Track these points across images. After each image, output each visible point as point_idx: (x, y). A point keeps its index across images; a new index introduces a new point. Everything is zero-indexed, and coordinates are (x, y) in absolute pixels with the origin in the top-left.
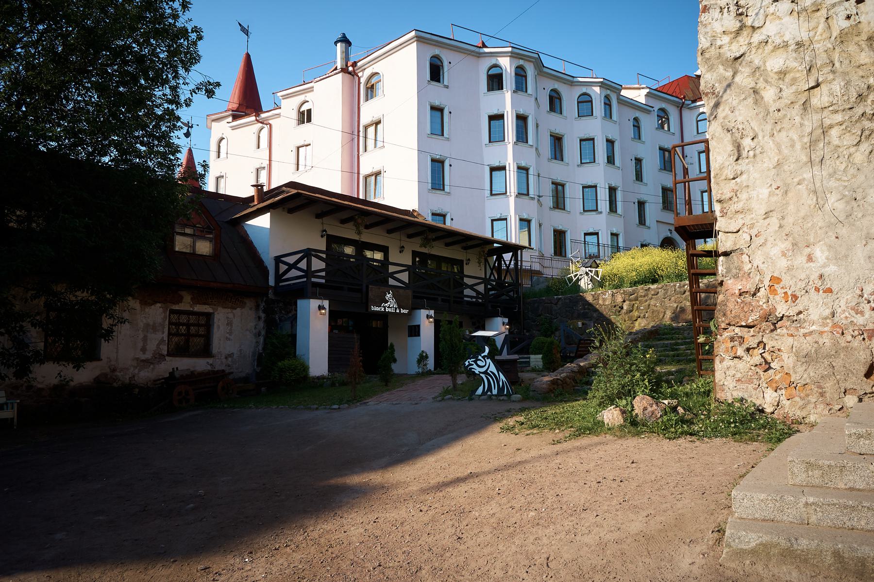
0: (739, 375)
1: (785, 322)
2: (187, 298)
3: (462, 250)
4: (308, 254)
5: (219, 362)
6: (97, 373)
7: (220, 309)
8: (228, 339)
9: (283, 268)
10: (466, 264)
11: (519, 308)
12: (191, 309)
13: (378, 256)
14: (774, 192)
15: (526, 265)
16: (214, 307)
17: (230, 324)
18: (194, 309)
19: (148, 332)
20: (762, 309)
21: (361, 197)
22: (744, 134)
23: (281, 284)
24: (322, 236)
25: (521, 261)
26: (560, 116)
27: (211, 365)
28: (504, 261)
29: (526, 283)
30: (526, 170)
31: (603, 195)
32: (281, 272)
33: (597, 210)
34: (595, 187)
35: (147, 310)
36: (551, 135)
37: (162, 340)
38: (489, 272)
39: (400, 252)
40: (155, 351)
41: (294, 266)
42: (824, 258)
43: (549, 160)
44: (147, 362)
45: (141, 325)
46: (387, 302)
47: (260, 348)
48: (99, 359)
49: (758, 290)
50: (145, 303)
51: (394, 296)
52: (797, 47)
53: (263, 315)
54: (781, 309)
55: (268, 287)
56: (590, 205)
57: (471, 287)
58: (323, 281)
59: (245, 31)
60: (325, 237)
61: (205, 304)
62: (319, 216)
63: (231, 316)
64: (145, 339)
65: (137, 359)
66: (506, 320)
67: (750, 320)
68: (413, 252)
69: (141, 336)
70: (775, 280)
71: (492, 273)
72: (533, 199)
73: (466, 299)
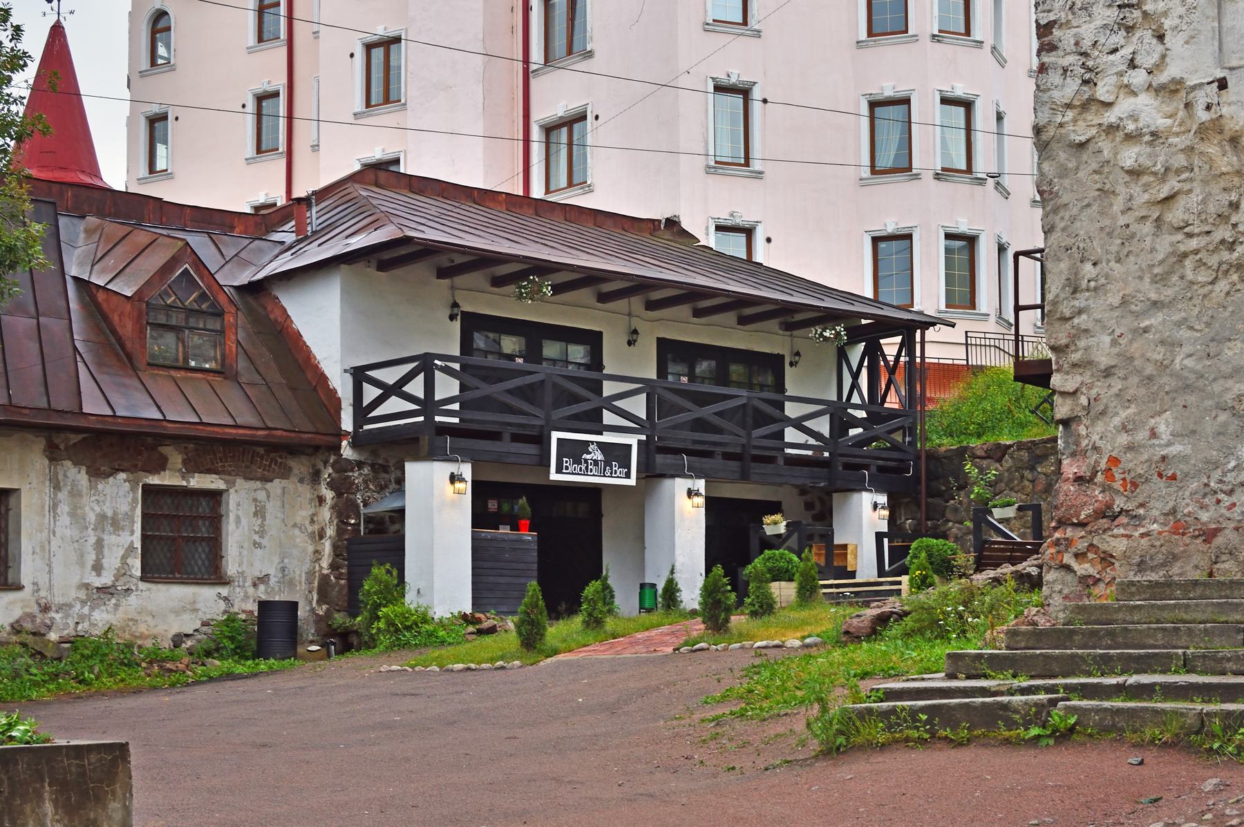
0: (1066, 591)
1: (1123, 519)
2: (176, 458)
3: (781, 332)
4: (425, 365)
5: (242, 594)
7: (240, 482)
8: (257, 545)
9: (371, 393)
10: (791, 364)
12: (184, 483)
13: (578, 353)
14: (1116, 340)
16: (227, 477)
17: (260, 512)
18: (188, 482)
19: (103, 531)
20: (1096, 501)
21: (537, 192)
22: (1085, 255)
23: (366, 427)
24: (452, 318)
25: (923, 342)
27: (226, 599)
28: (884, 356)
30: (967, 105)
35: (100, 487)
37: (131, 548)
38: (847, 381)
39: (630, 343)
40: (118, 570)
41: (395, 390)
42: (1168, 433)
44: (106, 591)
45: (92, 517)
47: (325, 563)
49: (1095, 473)
50: (96, 473)
52: (1151, 139)
53: (329, 495)
54: (1119, 503)
55: (340, 434)
57: (798, 424)
58: (456, 420)
60: (459, 317)
61: (209, 471)
62: (442, 273)
63: (261, 495)
64: (99, 545)
65: (87, 586)
67: (1082, 517)
68: (661, 342)
69: (92, 540)
70: (1114, 461)
72: (981, 182)
73: (788, 451)
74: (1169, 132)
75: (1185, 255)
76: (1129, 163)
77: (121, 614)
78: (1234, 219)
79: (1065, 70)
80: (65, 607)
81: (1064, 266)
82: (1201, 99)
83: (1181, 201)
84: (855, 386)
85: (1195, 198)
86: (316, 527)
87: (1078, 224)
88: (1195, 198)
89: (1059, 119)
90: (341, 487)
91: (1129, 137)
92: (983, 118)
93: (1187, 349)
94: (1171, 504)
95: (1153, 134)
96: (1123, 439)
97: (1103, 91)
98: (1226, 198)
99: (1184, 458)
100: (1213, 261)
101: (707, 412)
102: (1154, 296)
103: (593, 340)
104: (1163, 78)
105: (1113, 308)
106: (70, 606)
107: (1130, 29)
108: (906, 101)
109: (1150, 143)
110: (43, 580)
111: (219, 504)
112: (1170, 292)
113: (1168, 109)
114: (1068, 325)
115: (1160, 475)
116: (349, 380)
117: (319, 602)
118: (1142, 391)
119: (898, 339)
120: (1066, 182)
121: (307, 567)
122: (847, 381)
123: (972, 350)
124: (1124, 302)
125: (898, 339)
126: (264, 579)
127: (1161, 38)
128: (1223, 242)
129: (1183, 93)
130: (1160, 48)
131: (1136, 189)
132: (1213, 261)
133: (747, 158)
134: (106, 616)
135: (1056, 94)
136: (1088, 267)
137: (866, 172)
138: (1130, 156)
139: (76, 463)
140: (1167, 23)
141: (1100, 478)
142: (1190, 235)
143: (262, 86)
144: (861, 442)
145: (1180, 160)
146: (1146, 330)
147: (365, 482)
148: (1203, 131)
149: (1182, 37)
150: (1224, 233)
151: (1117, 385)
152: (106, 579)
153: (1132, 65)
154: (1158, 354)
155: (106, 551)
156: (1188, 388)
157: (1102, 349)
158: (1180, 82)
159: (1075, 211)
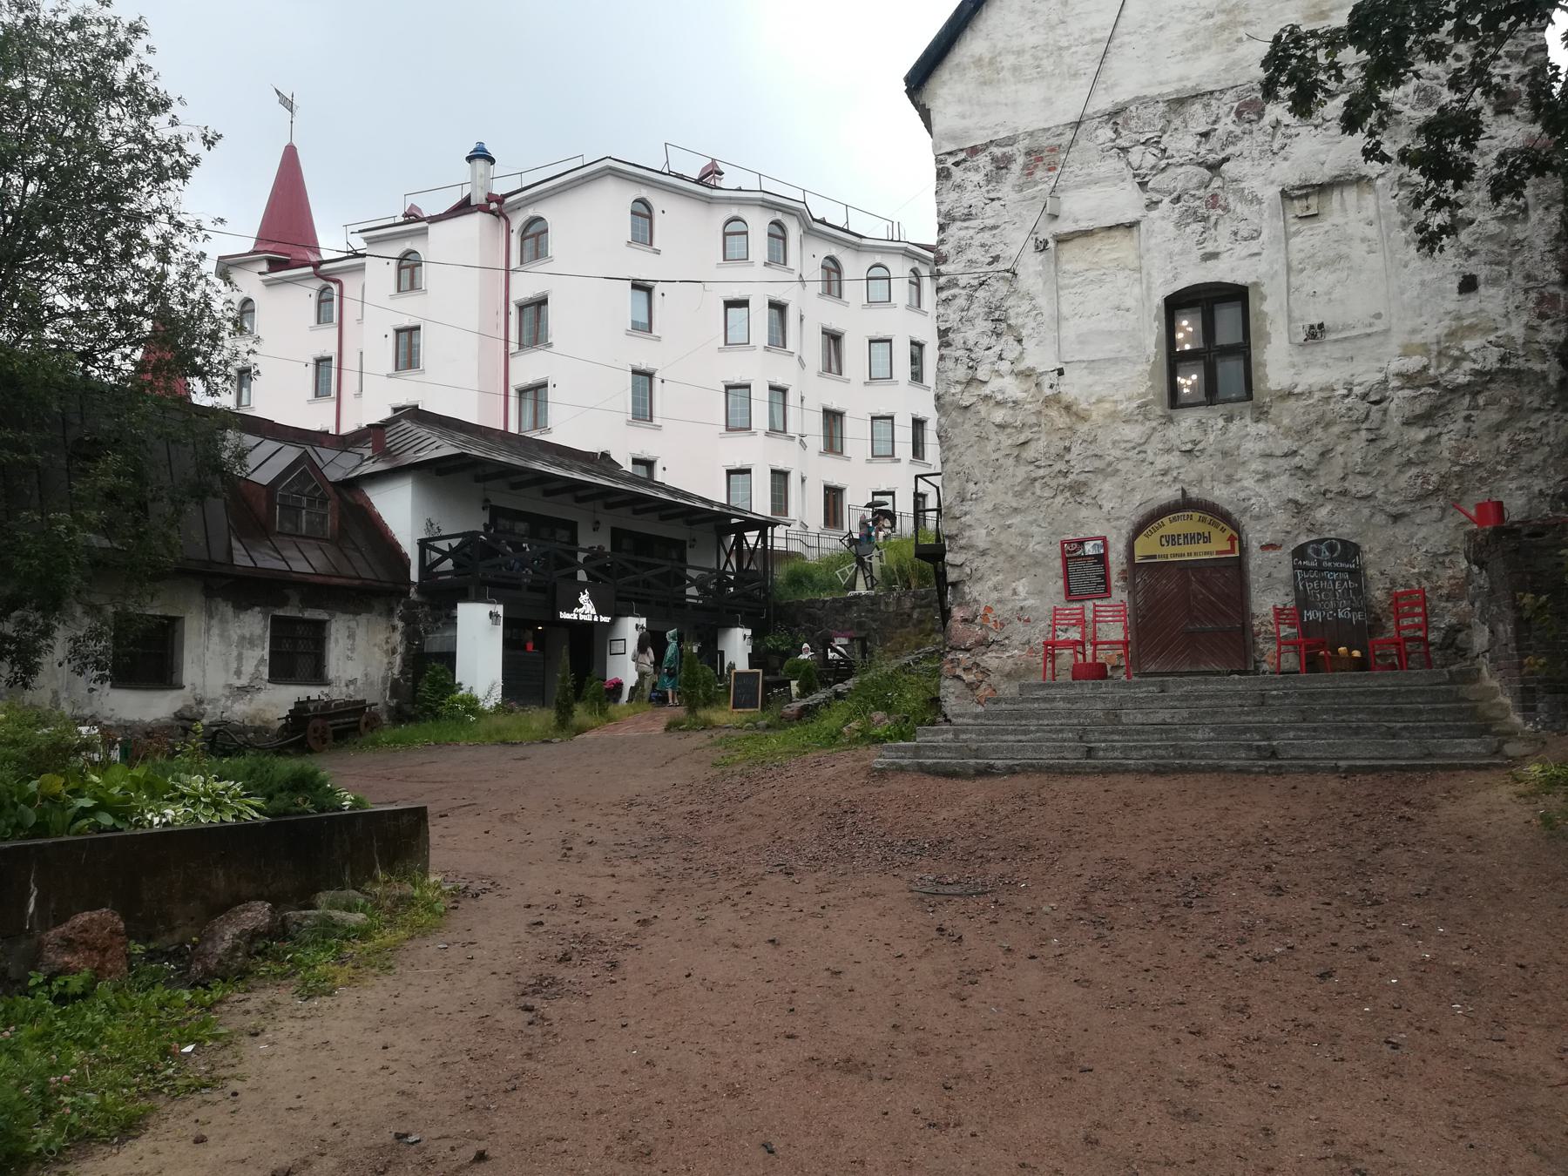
1: (994, 647)
6: (178, 706)
8: (349, 658)
11: (768, 615)
15: (779, 545)
25: (772, 537)
26: (838, 300)
29: (780, 573)
30: (784, 391)
31: (904, 435)
32: (428, 563)
33: (893, 455)
34: (892, 418)
36: (823, 333)
37: (262, 660)
38: (723, 558)
43: (820, 375)
44: (243, 690)
45: (235, 638)
46: (581, 606)
47: (396, 671)
48: (182, 687)
51: (591, 597)
53: (400, 624)
54: (992, 636)
55: (409, 583)
56: (884, 448)
59: (288, 104)
61: (318, 607)
62: (478, 479)
64: (240, 657)
65: (230, 686)
66: (749, 632)
69: (235, 653)
70: (988, 609)
71: (728, 561)
72: (792, 438)
74: (1024, 401)
75: (1035, 480)
76: (998, 420)
77: (253, 706)
78: (1067, 458)
79: (957, 360)
80: (213, 701)
81: (955, 484)
82: (1046, 381)
83: (1033, 445)
84: (728, 561)
85: (1042, 444)
86: (390, 646)
87: (964, 458)
88: (1042, 444)
89: (953, 391)
90: (410, 620)
91: (998, 403)
92: (792, 398)
93: (1037, 539)
94: (1026, 638)
95: (1014, 402)
96: (995, 595)
97: (982, 374)
98: (1062, 444)
99: (1035, 609)
100: (1054, 483)
101: (648, 574)
102: (1015, 505)
103: (572, 527)
104: (1021, 366)
105: (987, 512)
106: (218, 700)
107: (999, 335)
108: (748, 387)
109: (1012, 408)
110: (199, 681)
111: (324, 630)
112: (1025, 503)
113: (1025, 387)
114: (958, 522)
115: (1019, 619)
116: (417, 548)
117: (391, 697)
118: (1007, 565)
119: (757, 533)
120: (957, 431)
121: (382, 673)
122: (723, 558)
123: (790, 542)
124: (995, 508)
125: (757, 533)
126: (353, 682)
127: (1020, 341)
128: (1060, 472)
129: (1034, 377)
130: (1020, 348)
131: (1002, 437)
132: (1054, 483)
133: (651, 416)
134: (243, 707)
135: (950, 374)
136: (971, 486)
137: (723, 429)
138: (999, 416)
139: (226, 599)
140: (1024, 333)
141: (979, 620)
142: (1039, 467)
143: (319, 352)
144: (733, 596)
145: (1033, 419)
146: (1009, 526)
147: (426, 616)
148: (1048, 402)
149: (1034, 341)
150: (1061, 466)
151: (990, 561)
152: (244, 681)
153: (1001, 358)
154: (1018, 542)
155: (244, 661)
156: (1037, 563)
157: (980, 537)
158: (1033, 370)
159: (962, 450)
